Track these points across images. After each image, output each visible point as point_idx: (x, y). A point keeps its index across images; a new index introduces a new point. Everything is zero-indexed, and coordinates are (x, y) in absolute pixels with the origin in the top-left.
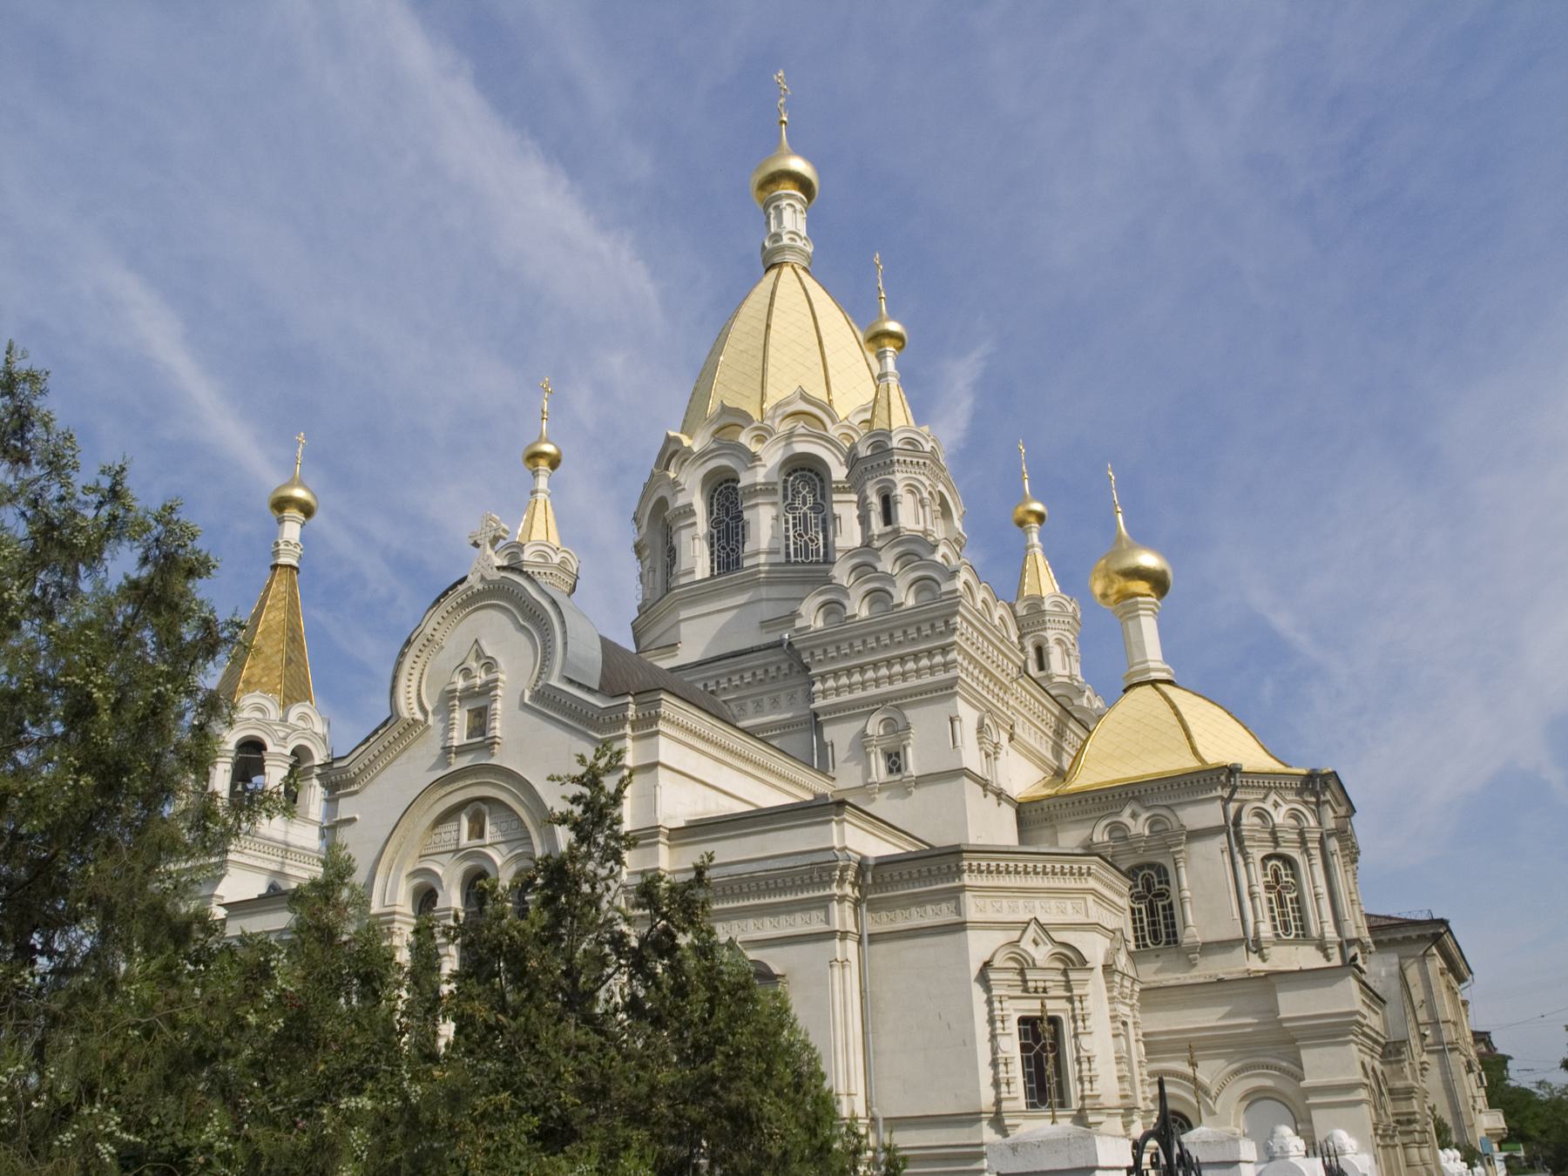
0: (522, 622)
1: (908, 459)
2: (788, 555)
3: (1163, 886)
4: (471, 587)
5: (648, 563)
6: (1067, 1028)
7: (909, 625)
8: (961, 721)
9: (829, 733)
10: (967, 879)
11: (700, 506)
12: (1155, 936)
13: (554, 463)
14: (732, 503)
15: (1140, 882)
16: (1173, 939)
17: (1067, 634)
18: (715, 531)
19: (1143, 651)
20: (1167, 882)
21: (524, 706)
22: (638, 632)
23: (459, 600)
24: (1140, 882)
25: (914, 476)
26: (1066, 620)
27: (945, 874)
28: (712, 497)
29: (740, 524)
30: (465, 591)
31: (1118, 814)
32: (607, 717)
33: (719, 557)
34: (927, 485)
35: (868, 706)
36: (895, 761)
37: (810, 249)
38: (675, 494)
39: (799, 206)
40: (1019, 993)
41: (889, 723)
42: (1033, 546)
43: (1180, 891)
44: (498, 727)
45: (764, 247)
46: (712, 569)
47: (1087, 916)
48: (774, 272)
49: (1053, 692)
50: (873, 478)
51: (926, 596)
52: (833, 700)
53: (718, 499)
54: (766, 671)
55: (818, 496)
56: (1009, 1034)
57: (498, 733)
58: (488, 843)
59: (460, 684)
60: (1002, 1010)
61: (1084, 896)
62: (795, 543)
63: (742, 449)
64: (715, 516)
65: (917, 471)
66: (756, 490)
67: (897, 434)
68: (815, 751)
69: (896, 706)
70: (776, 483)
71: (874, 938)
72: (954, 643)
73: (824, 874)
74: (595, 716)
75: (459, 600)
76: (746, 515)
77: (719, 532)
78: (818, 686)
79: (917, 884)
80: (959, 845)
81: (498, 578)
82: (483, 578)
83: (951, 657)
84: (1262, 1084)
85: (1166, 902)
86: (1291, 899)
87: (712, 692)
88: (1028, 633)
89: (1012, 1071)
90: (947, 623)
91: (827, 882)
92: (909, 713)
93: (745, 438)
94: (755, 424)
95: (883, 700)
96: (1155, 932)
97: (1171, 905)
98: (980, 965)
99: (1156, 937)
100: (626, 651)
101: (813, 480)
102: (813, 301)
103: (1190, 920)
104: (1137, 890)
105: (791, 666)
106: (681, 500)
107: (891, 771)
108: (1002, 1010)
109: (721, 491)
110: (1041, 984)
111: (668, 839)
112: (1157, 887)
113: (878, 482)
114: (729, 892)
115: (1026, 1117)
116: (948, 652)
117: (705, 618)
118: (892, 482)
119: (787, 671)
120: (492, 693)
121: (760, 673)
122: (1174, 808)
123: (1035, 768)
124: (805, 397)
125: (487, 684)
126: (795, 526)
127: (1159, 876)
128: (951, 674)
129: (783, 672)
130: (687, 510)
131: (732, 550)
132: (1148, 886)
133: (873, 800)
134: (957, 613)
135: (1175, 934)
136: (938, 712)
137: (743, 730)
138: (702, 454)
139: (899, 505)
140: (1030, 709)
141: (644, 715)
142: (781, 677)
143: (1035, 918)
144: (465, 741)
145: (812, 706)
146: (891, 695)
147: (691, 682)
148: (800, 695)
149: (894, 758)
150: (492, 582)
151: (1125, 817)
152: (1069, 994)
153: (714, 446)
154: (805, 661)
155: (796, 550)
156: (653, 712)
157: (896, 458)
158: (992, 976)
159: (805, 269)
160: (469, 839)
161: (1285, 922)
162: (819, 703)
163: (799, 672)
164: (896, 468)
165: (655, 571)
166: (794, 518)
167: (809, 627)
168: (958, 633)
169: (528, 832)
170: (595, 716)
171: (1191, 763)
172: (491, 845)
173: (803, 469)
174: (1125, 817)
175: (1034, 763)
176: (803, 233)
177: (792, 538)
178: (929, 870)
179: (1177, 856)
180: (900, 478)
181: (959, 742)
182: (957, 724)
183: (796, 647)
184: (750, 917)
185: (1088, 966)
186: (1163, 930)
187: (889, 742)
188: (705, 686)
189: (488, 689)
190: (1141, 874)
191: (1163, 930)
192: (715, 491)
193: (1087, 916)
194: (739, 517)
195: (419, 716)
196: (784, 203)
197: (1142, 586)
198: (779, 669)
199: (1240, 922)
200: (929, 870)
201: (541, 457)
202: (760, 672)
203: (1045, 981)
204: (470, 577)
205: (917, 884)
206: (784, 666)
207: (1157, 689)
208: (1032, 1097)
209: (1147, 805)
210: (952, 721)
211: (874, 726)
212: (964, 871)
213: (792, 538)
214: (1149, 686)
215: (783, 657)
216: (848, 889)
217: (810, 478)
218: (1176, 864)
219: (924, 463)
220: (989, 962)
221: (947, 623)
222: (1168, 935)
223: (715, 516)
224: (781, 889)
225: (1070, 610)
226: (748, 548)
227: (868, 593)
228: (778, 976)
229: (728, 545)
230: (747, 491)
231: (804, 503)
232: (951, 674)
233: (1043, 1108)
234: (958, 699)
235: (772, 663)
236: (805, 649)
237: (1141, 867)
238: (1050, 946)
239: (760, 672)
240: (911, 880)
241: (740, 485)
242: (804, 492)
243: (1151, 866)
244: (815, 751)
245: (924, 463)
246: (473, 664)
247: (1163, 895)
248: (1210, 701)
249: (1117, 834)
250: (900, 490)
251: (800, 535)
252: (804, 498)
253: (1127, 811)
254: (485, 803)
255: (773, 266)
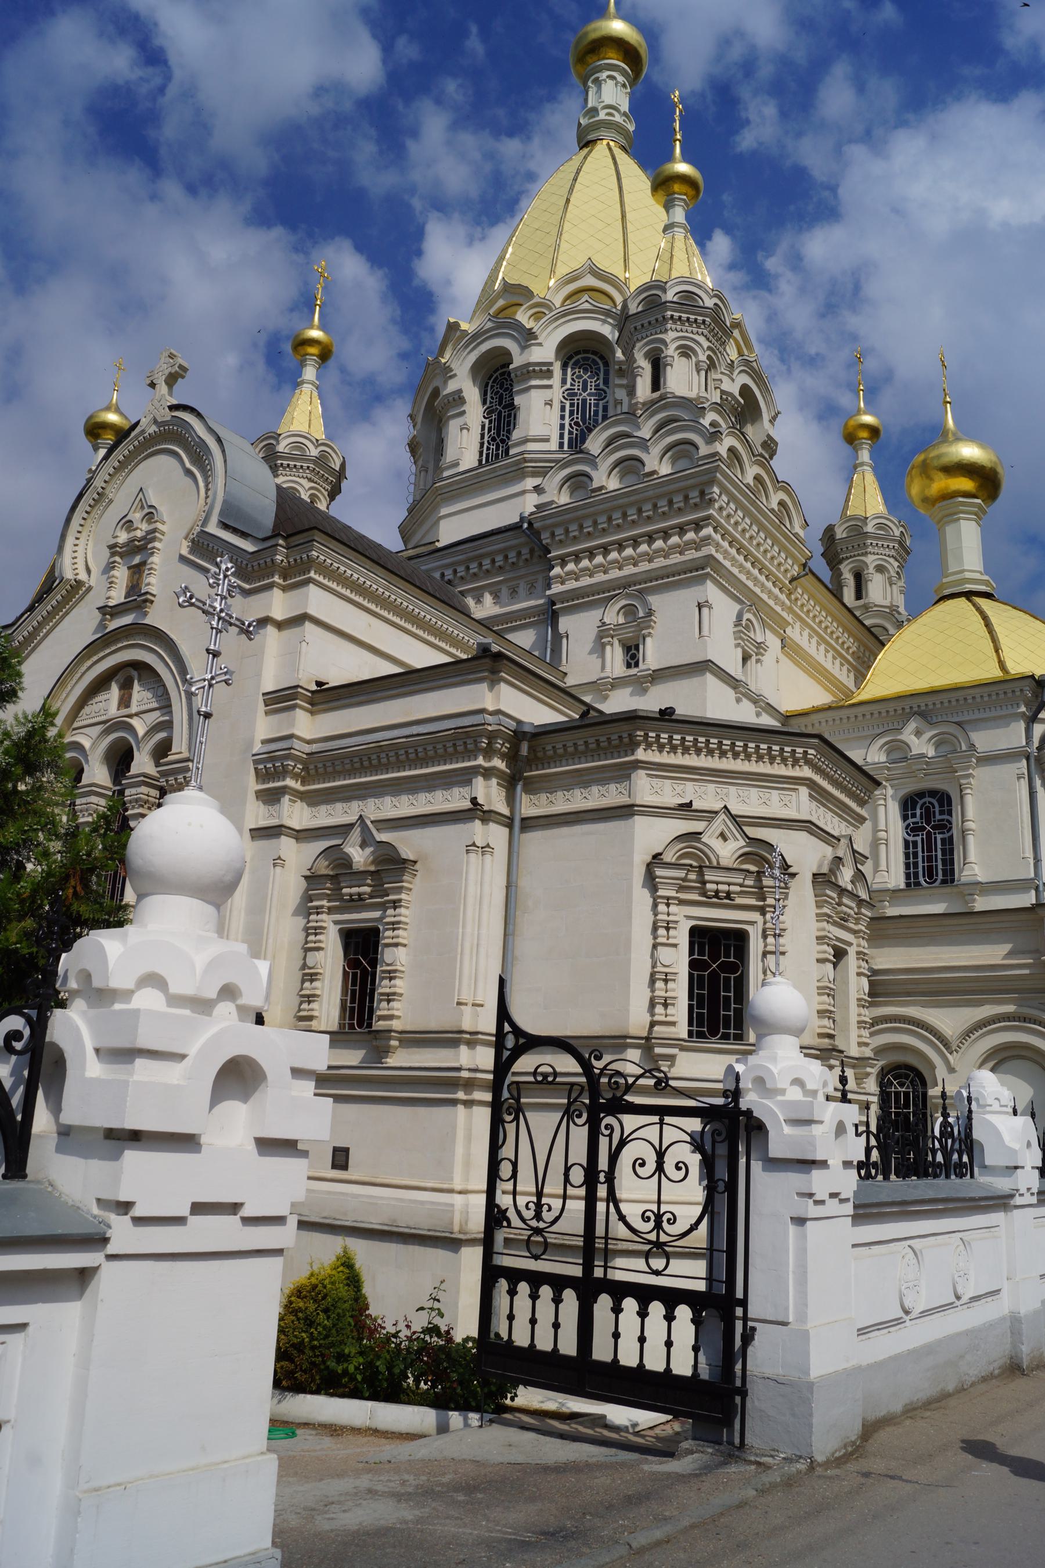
0: (188, 465)
1: (685, 316)
2: (561, 445)
3: (946, 817)
4: (143, 432)
5: (420, 463)
6: (755, 946)
7: (660, 496)
8: (710, 607)
9: (565, 623)
10: (641, 754)
11: (472, 394)
12: (930, 873)
13: (325, 355)
14: (506, 390)
15: (918, 812)
16: (949, 877)
17: (891, 560)
18: (487, 421)
19: (960, 559)
20: (950, 813)
21: (183, 559)
22: (405, 531)
23: (131, 447)
24: (918, 812)
25: (691, 335)
26: (891, 545)
27: (616, 747)
28: (487, 385)
29: (513, 412)
30: (136, 437)
31: (899, 730)
32: (255, 564)
33: (488, 449)
34: (896, 566)
35: (604, 593)
36: (632, 654)
37: (631, 127)
38: (445, 383)
39: (620, 79)
40: (695, 897)
41: (629, 611)
42: (862, 464)
43: (963, 822)
44: (153, 583)
45: (580, 124)
46: (480, 461)
47: (798, 811)
48: (586, 150)
49: (867, 622)
50: (643, 338)
51: (682, 464)
52: (571, 585)
53: (492, 387)
54: (506, 557)
55: (601, 381)
56: (675, 946)
57: (153, 590)
58: (133, 712)
59: (123, 537)
60: (666, 992)
61: (796, 787)
62: (570, 433)
63: (518, 326)
64: (488, 404)
65: (695, 330)
66: (528, 372)
67: (672, 287)
68: (549, 644)
69: (639, 591)
70: (551, 364)
71: (529, 824)
72: (709, 517)
73: (469, 741)
74: (245, 562)
75: (131, 447)
76: (518, 400)
77: (490, 422)
78: (557, 570)
79: (583, 759)
80: (635, 710)
81: (169, 418)
82: (155, 421)
83: (704, 532)
84: (1024, 1040)
85: (946, 835)
86: (914, 816)
87: (449, 582)
88: (847, 558)
89: (673, 990)
90: (702, 494)
91: (471, 751)
92: (654, 600)
93: (523, 317)
94: (536, 300)
95: (625, 584)
96: (930, 868)
97: (951, 838)
98: (649, 859)
99: (930, 876)
100: (306, 502)
101: (598, 364)
102: (622, 175)
103: (972, 856)
104: (914, 820)
105: (532, 551)
106: (452, 386)
107: (629, 666)
108: (668, 914)
109: (497, 378)
110: (725, 888)
111: (312, 705)
112: (938, 817)
113: (646, 344)
114: (366, 763)
115: (683, 1049)
116: (702, 528)
117: (466, 514)
118: (663, 342)
119: (528, 556)
120: (150, 546)
121: (499, 559)
122: (964, 726)
123: (819, 688)
124: (595, 272)
125: (148, 533)
126: (571, 413)
127: (941, 805)
128: (705, 551)
129: (524, 557)
130: (456, 397)
131: (503, 441)
132: (928, 815)
133: (606, 697)
134: (712, 482)
135: (952, 871)
136: (689, 596)
137: (494, 632)
138: (476, 336)
139: (869, 583)
140: (864, 662)
141: (295, 560)
142: (521, 564)
143: (725, 807)
144: (122, 600)
145: (548, 593)
146: (633, 579)
147: (427, 571)
148: (539, 585)
149: (633, 651)
150: (164, 423)
151: (908, 735)
152: (761, 903)
153: (490, 325)
154: (544, 542)
155: (570, 440)
156: (304, 556)
157: (669, 313)
158: (659, 872)
159: (623, 148)
160: (118, 709)
161: (930, 850)
162: (556, 589)
163: (540, 556)
164: (669, 326)
165: (427, 471)
166: (572, 405)
167: (552, 502)
168: (717, 505)
169: (169, 699)
170: (245, 562)
171: (997, 673)
172: (137, 714)
173: (586, 351)
174: (908, 735)
175: (819, 682)
176: (625, 107)
177: (567, 427)
178: (597, 741)
179: (963, 781)
180: (672, 337)
181: (705, 632)
182: (705, 610)
183: (535, 525)
184: (387, 794)
185: (791, 870)
186: (940, 867)
187: (628, 634)
188: (443, 575)
189: (150, 537)
190: (921, 802)
191: (940, 867)
192: (490, 379)
193: (798, 811)
194: (511, 407)
195: (83, 576)
196: (604, 75)
197: (965, 484)
198: (519, 554)
199: (1032, 861)
200: (597, 741)
201: (310, 345)
202: (499, 558)
203: (729, 884)
204: (143, 420)
205: (583, 759)
206: (525, 551)
207: (970, 601)
208: (700, 1024)
209: (935, 720)
210: (700, 606)
211: (613, 615)
212: (638, 745)
213: (567, 427)
214: (964, 599)
215: (523, 540)
216: (498, 763)
217: (594, 361)
218: (961, 791)
219: (704, 321)
220: (661, 854)
221: (702, 494)
222: (944, 872)
223: (568, 386)
224: (423, 759)
225: (897, 533)
226: (516, 435)
227: (617, 464)
228: (405, 861)
229: (499, 436)
230: (519, 373)
231: (585, 389)
232: (705, 551)
233: (713, 1040)
234: (708, 582)
235: (511, 548)
236: (545, 528)
237: (921, 794)
238: (742, 843)
239: (499, 558)
240: (577, 755)
241: (511, 367)
242: (585, 377)
243: (933, 793)
244: (549, 644)
245: (704, 321)
246: (137, 516)
247: (945, 827)
248: (1032, 616)
249: (896, 755)
250: (671, 351)
251: (577, 424)
252: (585, 383)
253: (912, 725)
254: (135, 669)
255: (587, 144)
